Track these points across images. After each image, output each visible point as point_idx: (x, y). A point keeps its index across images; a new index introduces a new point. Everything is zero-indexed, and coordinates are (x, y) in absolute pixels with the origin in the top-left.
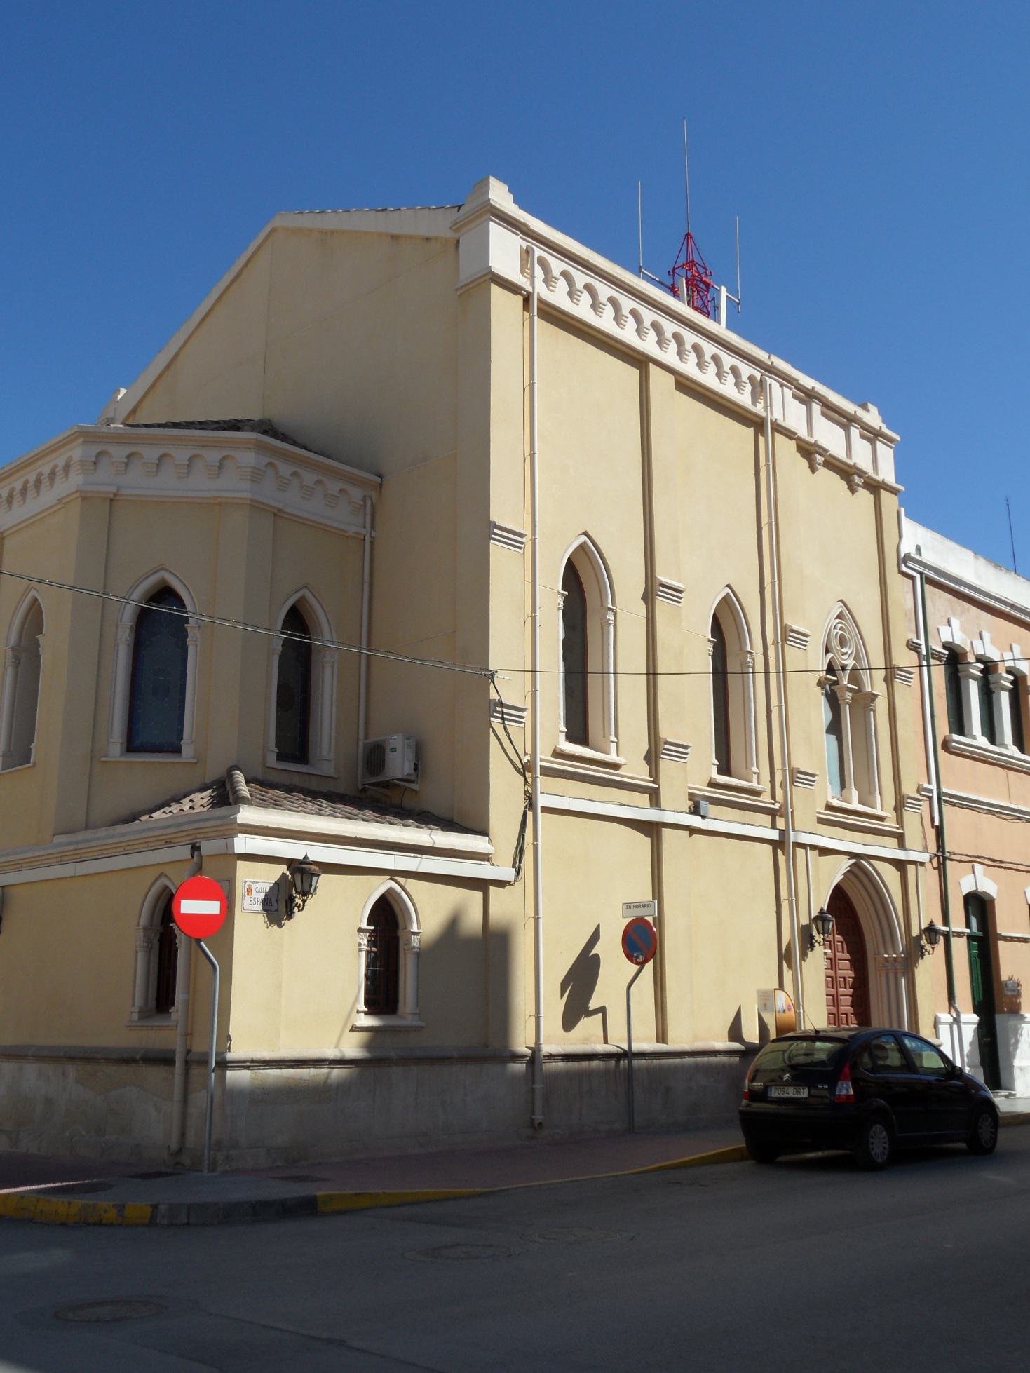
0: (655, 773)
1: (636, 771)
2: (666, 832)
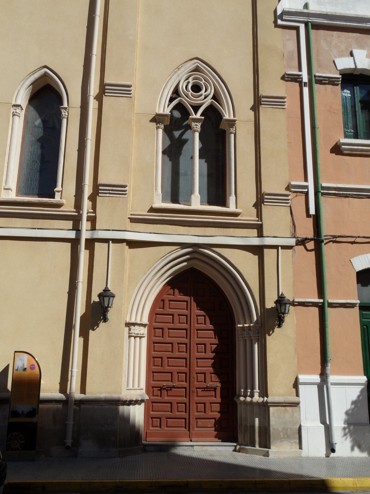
0: (259, 215)
1: (249, 216)
2: (266, 251)
